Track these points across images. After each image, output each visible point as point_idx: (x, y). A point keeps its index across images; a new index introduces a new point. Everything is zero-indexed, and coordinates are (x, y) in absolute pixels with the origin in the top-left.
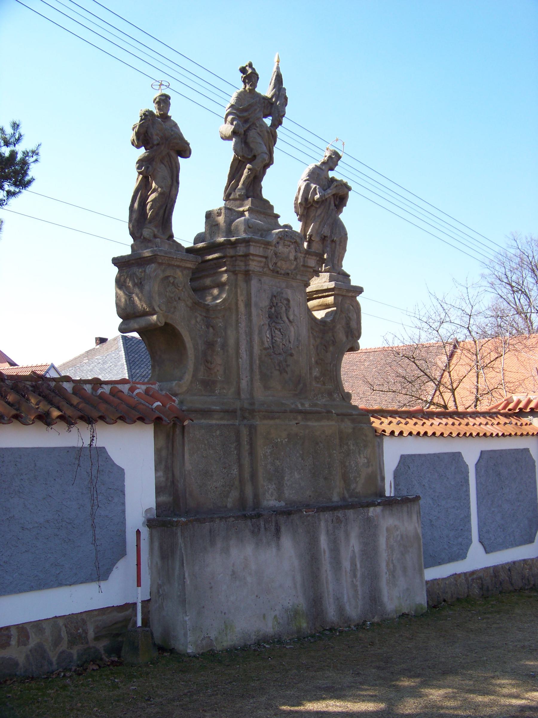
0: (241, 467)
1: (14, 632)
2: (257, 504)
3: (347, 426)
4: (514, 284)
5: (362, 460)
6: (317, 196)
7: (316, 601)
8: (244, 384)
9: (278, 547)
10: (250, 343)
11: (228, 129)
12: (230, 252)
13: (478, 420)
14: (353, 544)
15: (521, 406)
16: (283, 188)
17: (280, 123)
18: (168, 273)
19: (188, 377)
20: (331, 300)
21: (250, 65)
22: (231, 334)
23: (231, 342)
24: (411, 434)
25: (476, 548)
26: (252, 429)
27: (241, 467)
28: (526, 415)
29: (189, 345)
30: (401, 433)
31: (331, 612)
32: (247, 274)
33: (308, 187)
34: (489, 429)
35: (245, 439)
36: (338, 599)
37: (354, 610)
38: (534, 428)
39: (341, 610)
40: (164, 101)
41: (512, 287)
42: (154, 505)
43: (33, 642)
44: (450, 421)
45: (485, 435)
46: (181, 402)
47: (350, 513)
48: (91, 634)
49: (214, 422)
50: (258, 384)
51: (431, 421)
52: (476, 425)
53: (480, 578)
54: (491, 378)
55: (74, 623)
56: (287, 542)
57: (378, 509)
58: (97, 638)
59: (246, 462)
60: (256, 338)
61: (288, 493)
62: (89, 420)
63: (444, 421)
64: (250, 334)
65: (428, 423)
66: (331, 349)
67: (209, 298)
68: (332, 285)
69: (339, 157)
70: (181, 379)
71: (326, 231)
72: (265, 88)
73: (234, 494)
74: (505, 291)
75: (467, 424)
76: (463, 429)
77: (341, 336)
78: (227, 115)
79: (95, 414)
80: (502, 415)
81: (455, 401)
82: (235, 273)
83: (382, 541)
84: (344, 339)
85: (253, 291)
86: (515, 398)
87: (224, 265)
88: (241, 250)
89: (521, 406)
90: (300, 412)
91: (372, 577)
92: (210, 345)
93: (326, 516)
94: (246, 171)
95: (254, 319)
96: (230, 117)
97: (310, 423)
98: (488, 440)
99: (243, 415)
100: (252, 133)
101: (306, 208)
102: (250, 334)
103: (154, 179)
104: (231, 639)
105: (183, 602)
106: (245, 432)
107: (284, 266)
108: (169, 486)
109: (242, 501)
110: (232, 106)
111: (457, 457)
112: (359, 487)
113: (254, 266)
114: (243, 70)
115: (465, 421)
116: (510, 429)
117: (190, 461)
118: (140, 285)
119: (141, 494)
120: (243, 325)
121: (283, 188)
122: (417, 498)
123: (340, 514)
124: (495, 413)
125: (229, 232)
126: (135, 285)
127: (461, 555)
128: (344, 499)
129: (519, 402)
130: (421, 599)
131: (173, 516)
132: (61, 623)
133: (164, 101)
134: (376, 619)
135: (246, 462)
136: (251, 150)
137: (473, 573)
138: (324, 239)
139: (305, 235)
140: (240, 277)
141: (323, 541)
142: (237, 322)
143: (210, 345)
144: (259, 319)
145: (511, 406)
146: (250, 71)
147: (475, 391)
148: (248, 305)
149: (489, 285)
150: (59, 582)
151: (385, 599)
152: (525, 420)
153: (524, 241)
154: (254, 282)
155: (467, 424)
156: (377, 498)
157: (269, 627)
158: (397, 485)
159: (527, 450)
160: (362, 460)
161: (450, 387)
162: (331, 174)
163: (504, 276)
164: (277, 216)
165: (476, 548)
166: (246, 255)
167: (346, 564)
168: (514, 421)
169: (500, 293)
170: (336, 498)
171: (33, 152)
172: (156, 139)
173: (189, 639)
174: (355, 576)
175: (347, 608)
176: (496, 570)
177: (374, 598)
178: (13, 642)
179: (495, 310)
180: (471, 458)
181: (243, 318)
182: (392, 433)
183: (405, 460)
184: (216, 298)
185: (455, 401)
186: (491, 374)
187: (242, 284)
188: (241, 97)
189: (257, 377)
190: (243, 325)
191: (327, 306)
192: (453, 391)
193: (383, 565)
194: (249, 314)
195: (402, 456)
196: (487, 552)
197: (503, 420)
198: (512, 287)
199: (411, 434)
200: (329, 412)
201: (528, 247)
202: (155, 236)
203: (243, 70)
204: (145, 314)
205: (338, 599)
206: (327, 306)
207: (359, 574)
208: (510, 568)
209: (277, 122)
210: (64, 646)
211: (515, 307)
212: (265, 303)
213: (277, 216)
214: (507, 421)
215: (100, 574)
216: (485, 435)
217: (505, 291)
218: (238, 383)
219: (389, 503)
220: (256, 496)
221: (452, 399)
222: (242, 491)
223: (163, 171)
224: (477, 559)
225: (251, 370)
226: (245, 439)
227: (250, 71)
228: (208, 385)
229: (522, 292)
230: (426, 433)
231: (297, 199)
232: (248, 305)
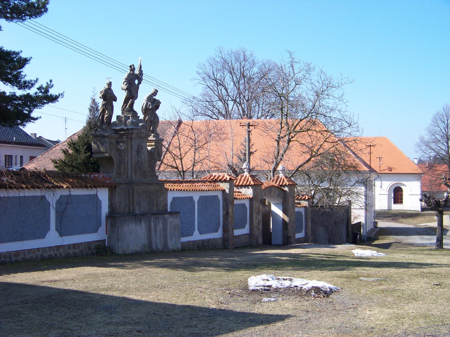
0: (129, 200)
1: (77, 245)
2: (134, 212)
3: (158, 187)
4: (218, 80)
5: (162, 199)
6: (150, 107)
7: (150, 242)
8: (129, 174)
9: (141, 225)
10: (132, 161)
11: (125, 87)
12: (127, 132)
13: (200, 184)
14: (160, 226)
15: (216, 178)
16: (139, 106)
17: (141, 83)
18: (111, 140)
19: (115, 172)
20: (153, 144)
21: (133, 65)
22: (126, 158)
23: (126, 161)
24: (177, 190)
25: (196, 232)
26: (133, 189)
27: (129, 200)
28: (218, 182)
29: (115, 162)
30: (174, 190)
31: (154, 247)
32: (131, 139)
33: (147, 104)
34: (203, 188)
35: (131, 192)
36: (156, 243)
37: (160, 247)
38: (220, 188)
39: (157, 246)
40: (110, 84)
41: (217, 82)
42: (108, 212)
43: (81, 248)
44: (189, 184)
45: (202, 190)
46: (114, 180)
47: (160, 216)
48: (93, 248)
49: (122, 187)
50: (133, 174)
51: (183, 185)
52: (199, 186)
53: (197, 243)
54: (202, 153)
55: (89, 244)
56: (143, 224)
57: (168, 215)
58: (94, 249)
59: (131, 199)
60: (133, 159)
61: (142, 209)
62: (95, 187)
63: (187, 184)
64: (132, 158)
65: (182, 185)
66: (153, 161)
67: (119, 147)
68: (154, 139)
69: (157, 91)
70: (112, 173)
71: (152, 119)
72: (137, 72)
73: (127, 209)
74: (211, 83)
75: (195, 186)
76: (194, 188)
77: (156, 156)
78: (124, 82)
79: (97, 185)
80: (208, 181)
81: (182, 165)
82: (128, 138)
83: (169, 226)
84: (157, 157)
85: (133, 144)
86: (214, 174)
87: (125, 136)
88: (131, 131)
89: (216, 178)
90: (145, 183)
91: (165, 237)
92: (120, 162)
93: (153, 217)
94: (130, 101)
95: (133, 153)
96: (125, 83)
97: (148, 187)
98: (203, 192)
99: (131, 184)
100: (132, 88)
101: (146, 111)
102: (132, 158)
103: (106, 110)
104: (128, 252)
105: (118, 239)
106: (131, 190)
107: (142, 135)
108: (111, 206)
109: (129, 211)
110: (126, 79)
111: (191, 198)
112: (161, 208)
113: (134, 136)
114: (131, 67)
115: (194, 184)
116: (211, 188)
117: (117, 199)
118: (102, 144)
119: (105, 209)
120: (129, 155)
121: (139, 106)
122: (179, 212)
123: (157, 216)
124: (205, 181)
125: (126, 124)
126: (100, 143)
127: (191, 234)
128: (156, 212)
129: (215, 176)
130: (179, 246)
131: (112, 215)
132: (86, 244)
133: (110, 84)
134: (166, 250)
135: (131, 199)
136: (132, 94)
137: (195, 241)
138: (151, 121)
139: (145, 120)
140: (129, 140)
141: (152, 224)
142: (128, 154)
143: (120, 162)
144: (134, 153)
145: (212, 178)
146: (133, 68)
147: (193, 160)
148: (131, 148)
149: (202, 79)
150: (83, 233)
151: (169, 245)
152: (217, 184)
153: (226, 53)
154: (133, 141)
155: (195, 186)
156: (165, 212)
157: (138, 249)
158: (171, 208)
159: (217, 196)
160: (162, 199)
161: (180, 157)
162: (154, 97)
163: (212, 75)
164: (139, 117)
165: (196, 232)
166: (132, 133)
167: (158, 232)
168: (213, 184)
169: (209, 85)
170: (155, 211)
171: (62, 94)
172: (108, 98)
173: (120, 250)
174: (160, 236)
175: (158, 246)
176: (203, 241)
177: (166, 244)
178: (77, 247)
179: (204, 95)
180: (196, 199)
181: (130, 152)
182: (171, 189)
183: (174, 199)
184: (121, 147)
185: (182, 165)
186: (202, 151)
187: (130, 142)
188: (129, 75)
189: (133, 172)
190: (129, 155)
191: (152, 146)
192: (181, 159)
193: (169, 233)
194: (132, 152)
195: (173, 198)
196: (200, 234)
197: (208, 184)
198: (217, 82)
199: (177, 190)
200: (153, 183)
201: (229, 57)
202: (107, 128)
203: (131, 67)
204: (104, 153)
205: (156, 243)
206: (152, 146)
207: (162, 235)
208: (209, 241)
209: (140, 83)
210: (87, 251)
211: (218, 95)
212: (136, 148)
213: (139, 117)
214: (210, 184)
215: (96, 231)
216: (202, 190)
217: (212, 83)
218: (128, 174)
219: (171, 213)
220: (133, 209)
221: (181, 164)
222: (129, 208)
223: (109, 107)
224: (197, 236)
225: (132, 170)
226: (131, 192)
227: (133, 68)
228: (120, 174)
229: (223, 86)
230: (181, 190)
231: (143, 107)
232: (131, 148)
